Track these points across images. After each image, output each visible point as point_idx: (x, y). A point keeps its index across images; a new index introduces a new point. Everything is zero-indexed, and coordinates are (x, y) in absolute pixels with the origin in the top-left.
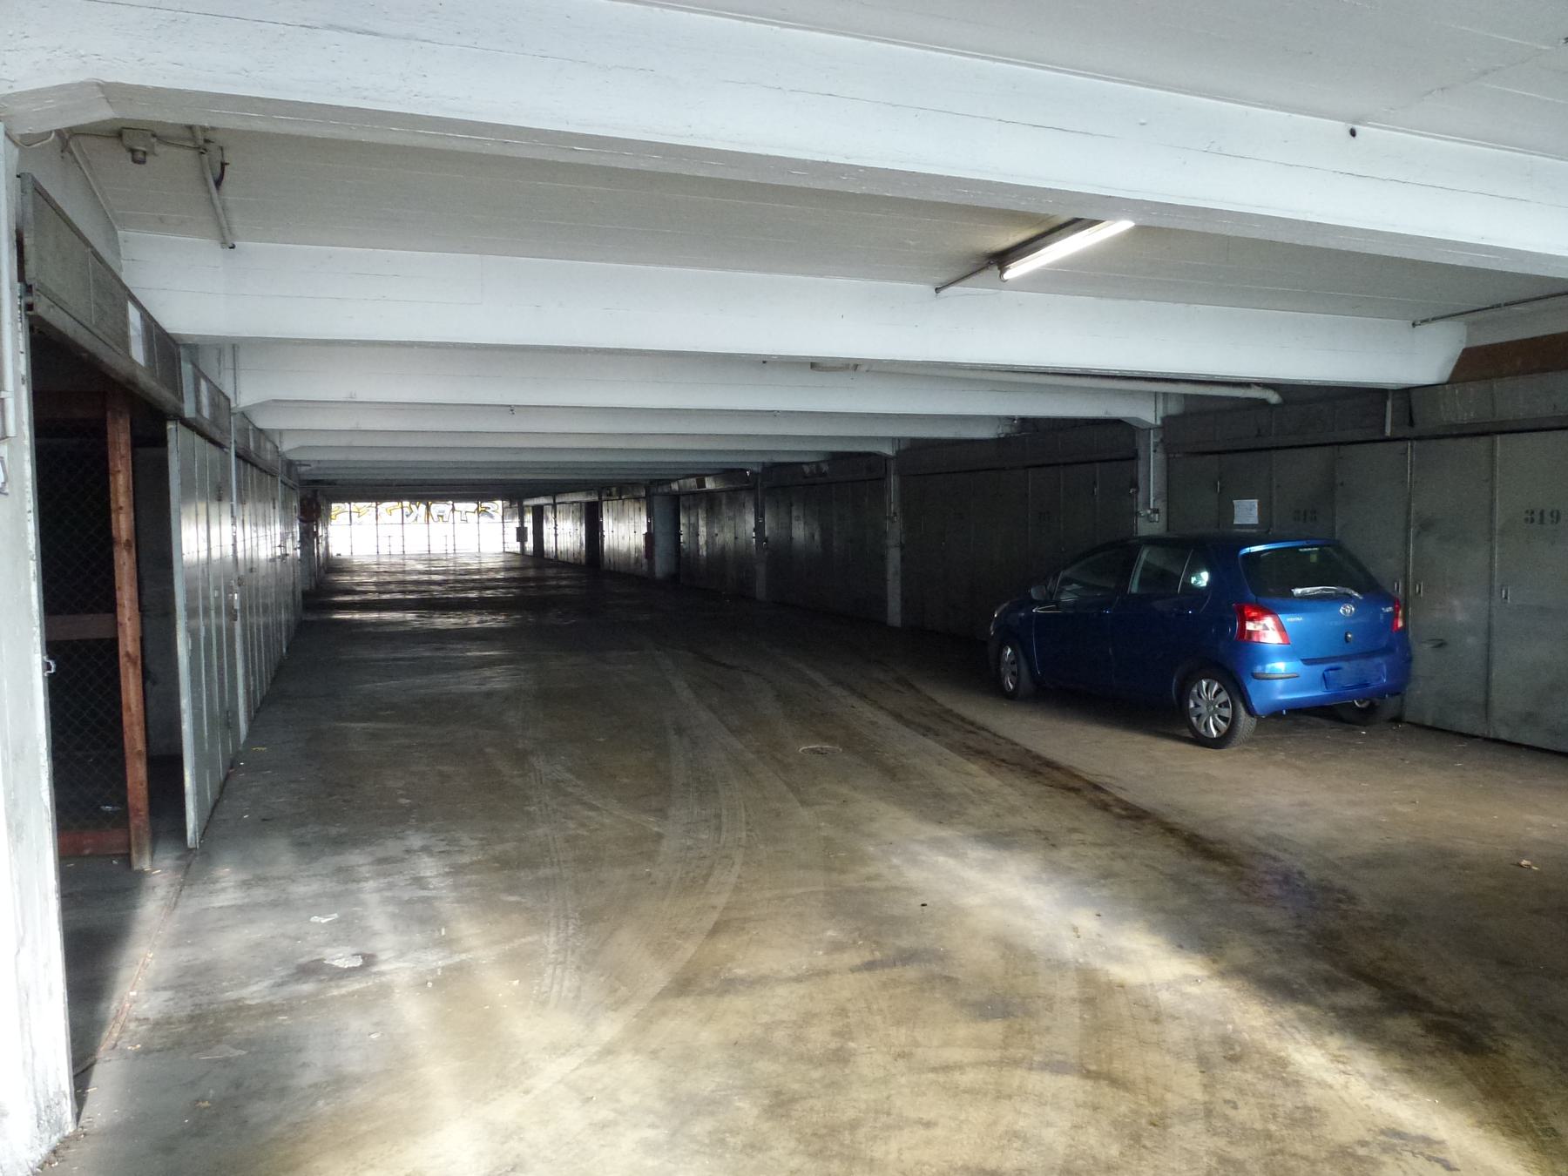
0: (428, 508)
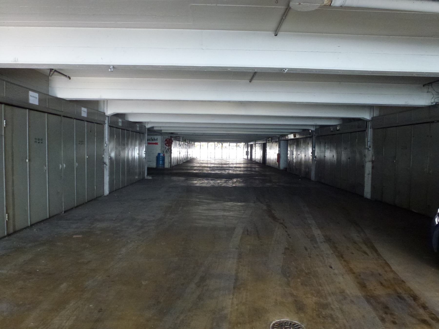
0: (222, 144)
